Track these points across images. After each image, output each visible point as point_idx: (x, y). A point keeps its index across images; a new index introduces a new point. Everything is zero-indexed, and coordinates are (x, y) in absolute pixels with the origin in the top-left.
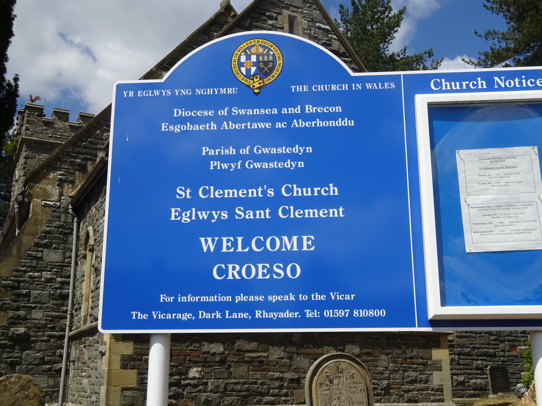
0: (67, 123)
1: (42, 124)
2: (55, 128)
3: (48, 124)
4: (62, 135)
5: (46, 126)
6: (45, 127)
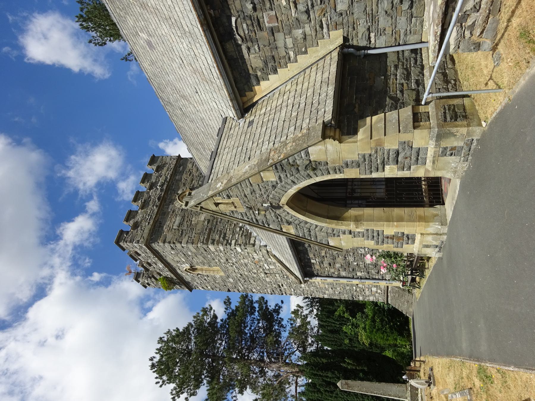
0: (139, 212)
1: (136, 231)
2: (142, 220)
3: (136, 226)
4: (149, 215)
5: (138, 227)
6: (139, 228)
